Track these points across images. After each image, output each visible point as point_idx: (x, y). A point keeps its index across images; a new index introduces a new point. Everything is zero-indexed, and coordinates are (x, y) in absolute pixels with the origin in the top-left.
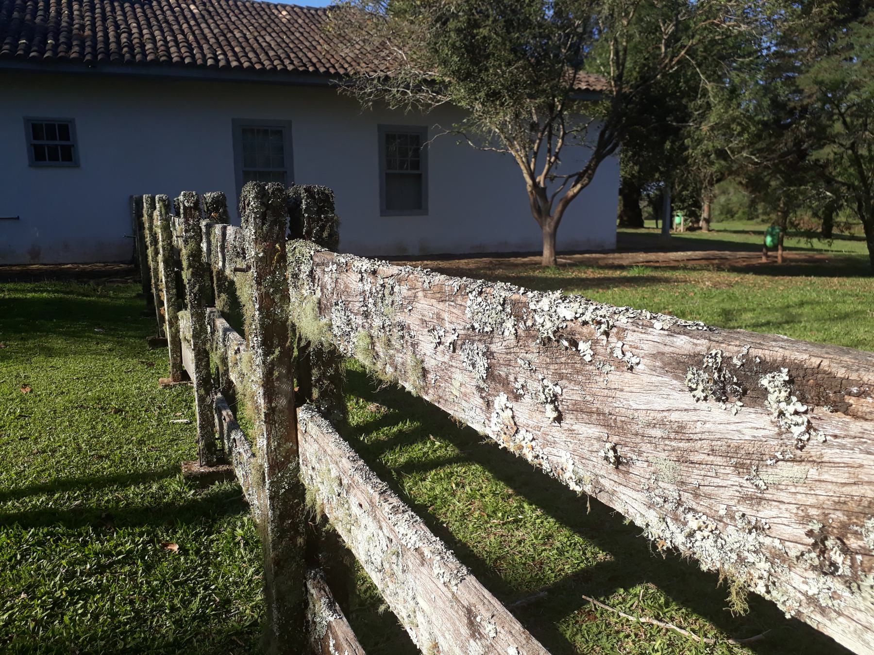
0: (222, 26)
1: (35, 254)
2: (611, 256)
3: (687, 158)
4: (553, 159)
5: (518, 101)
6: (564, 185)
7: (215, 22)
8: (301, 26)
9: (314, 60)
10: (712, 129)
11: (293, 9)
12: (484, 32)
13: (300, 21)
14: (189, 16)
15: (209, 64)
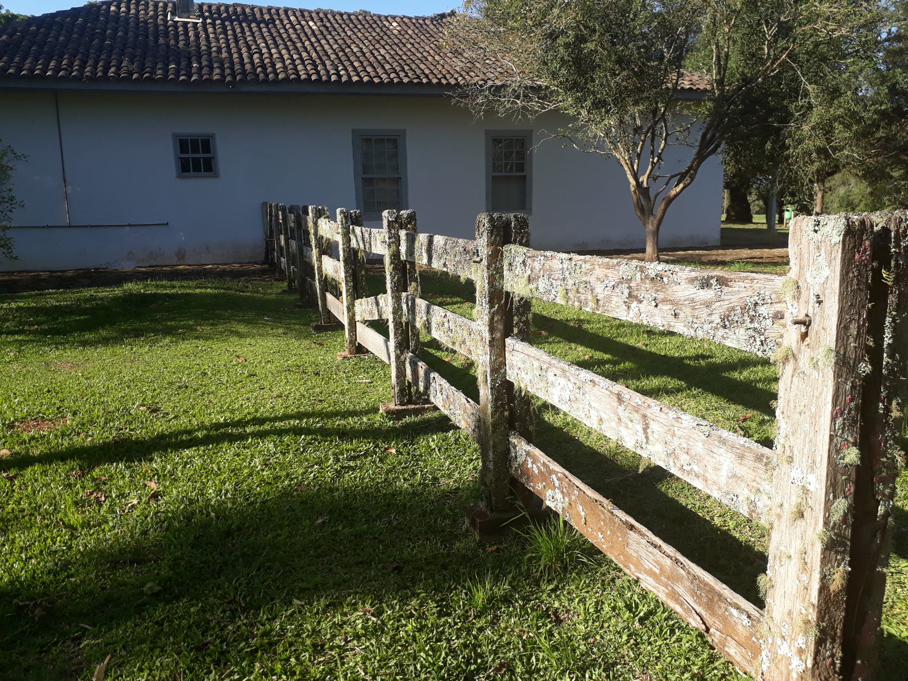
0: (340, 42)
1: (181, 256)
2: (715, 252)
3: (788, 157)
4: (656, 159)
5: (623, 109)
6: (667, 184)
7: (333, 38)
8: (411, 37)
9: (427, 71)
10: (813, 128)
11: (404, 21)
12: (591, 46)
13: (410, 32)
14: (309, 33)
15: (333, 80)
